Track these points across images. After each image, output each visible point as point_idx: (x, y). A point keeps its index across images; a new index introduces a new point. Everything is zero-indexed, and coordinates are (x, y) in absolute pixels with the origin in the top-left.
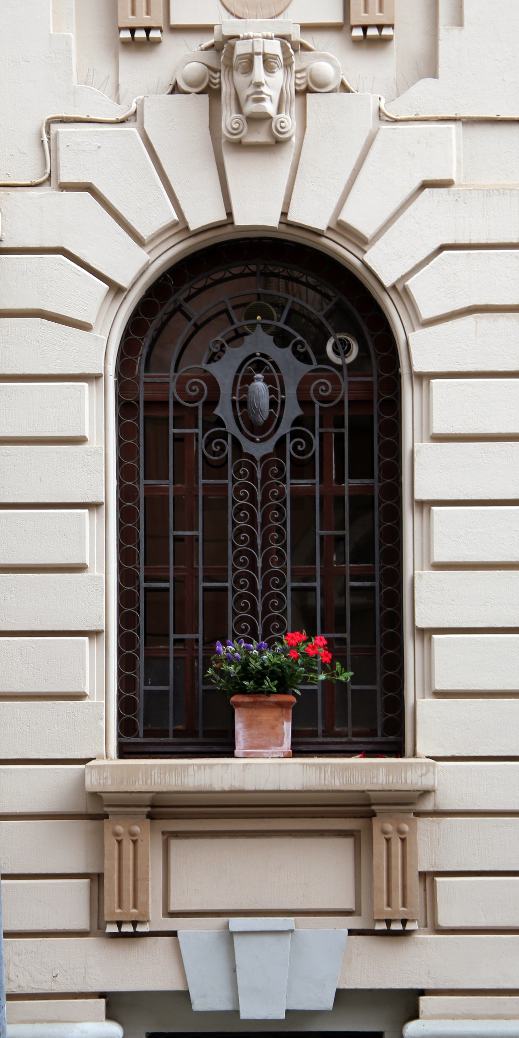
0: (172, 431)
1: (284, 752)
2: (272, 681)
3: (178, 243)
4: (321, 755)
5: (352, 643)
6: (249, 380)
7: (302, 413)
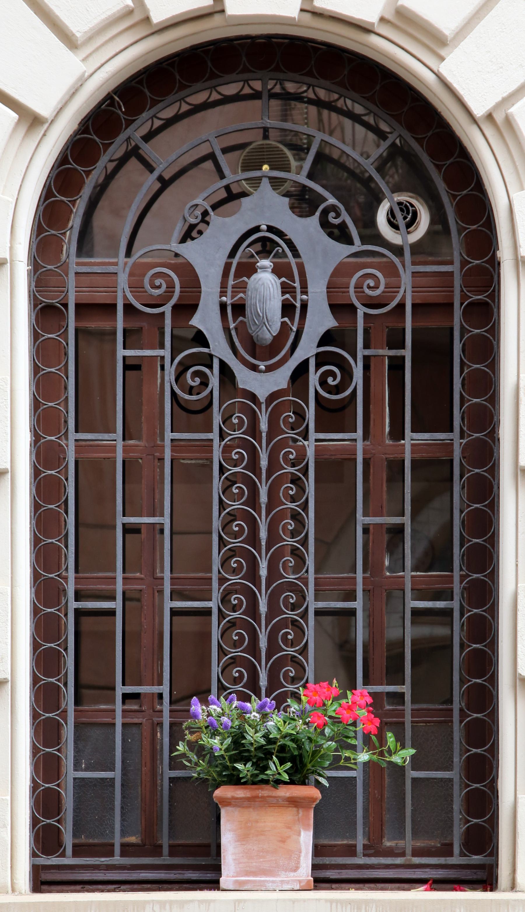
0: (121, 352)
1: (300, 882)
2: (281, 764)
3: (132, 45)
4: (361, 885)
5: (413, 702)
6: (248, 269)
7: (336, 324)
